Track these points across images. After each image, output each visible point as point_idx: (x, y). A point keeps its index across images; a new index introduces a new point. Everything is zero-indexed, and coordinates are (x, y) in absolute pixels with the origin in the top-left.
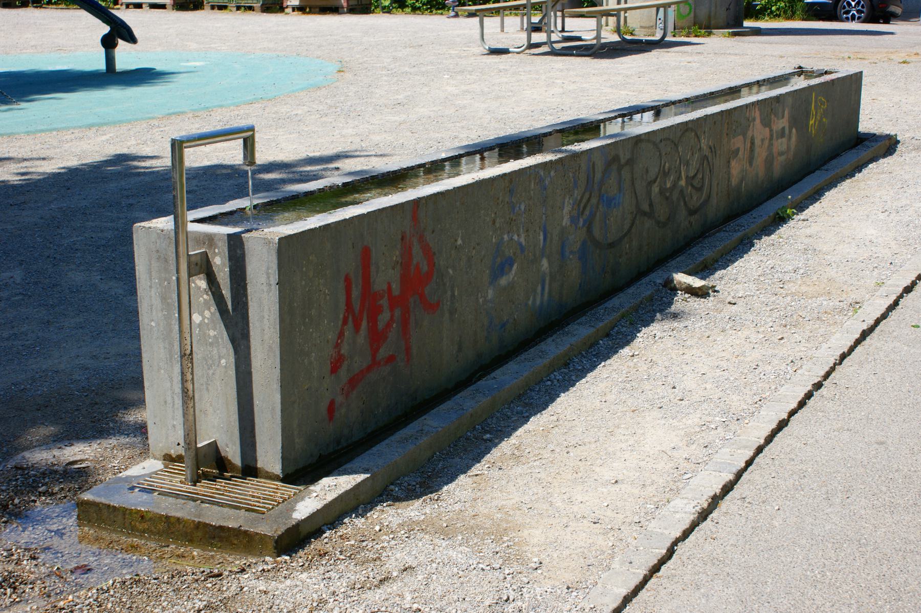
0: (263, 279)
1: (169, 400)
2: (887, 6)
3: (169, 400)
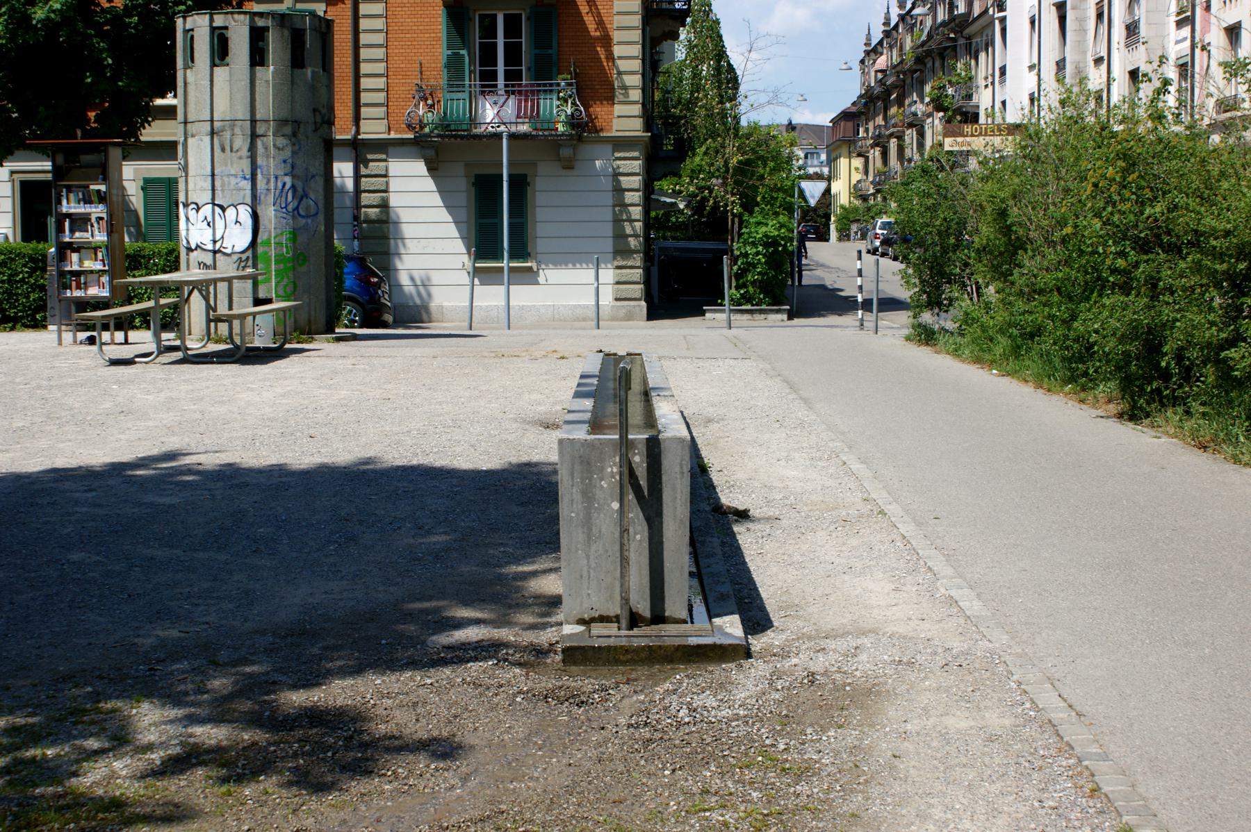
0: (677, 469)
1: (585, 574)
2: (381, 315)
3: (585, 574)
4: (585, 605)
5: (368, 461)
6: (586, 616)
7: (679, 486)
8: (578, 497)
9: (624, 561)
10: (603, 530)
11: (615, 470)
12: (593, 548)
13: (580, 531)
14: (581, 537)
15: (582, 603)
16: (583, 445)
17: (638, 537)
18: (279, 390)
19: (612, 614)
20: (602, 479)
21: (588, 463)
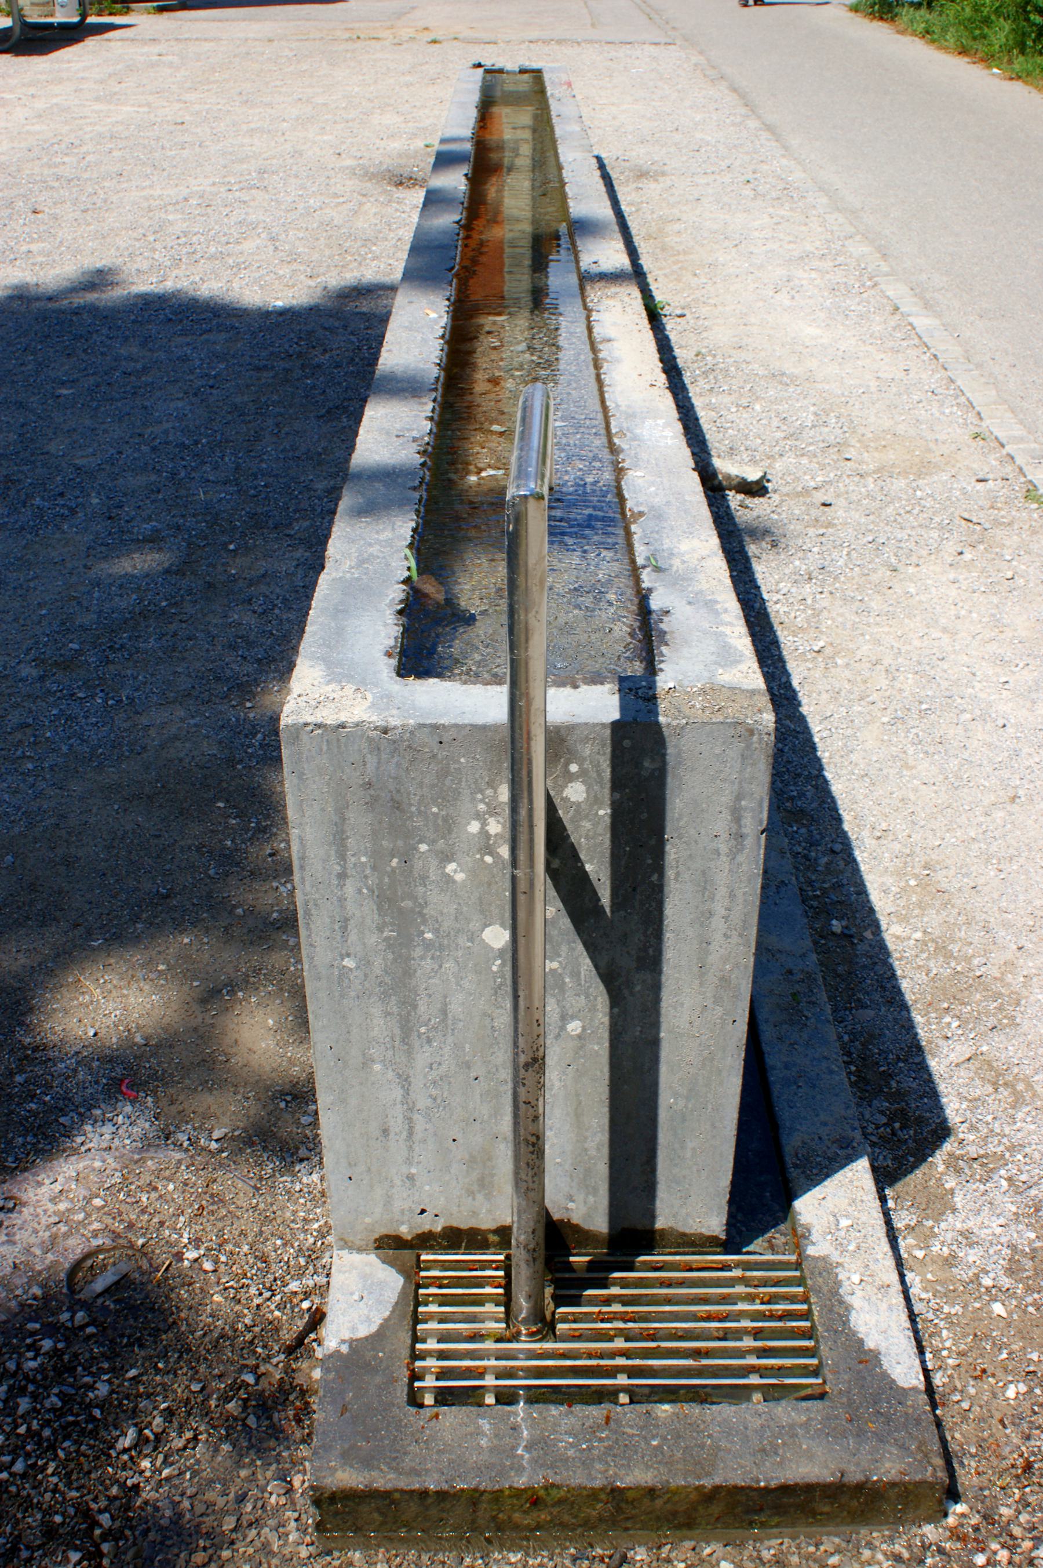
0: (721, 824)
1: (397, 1124)
4: (398, 1204)
5: (99, 279)
6: (405, 1231)
7: (722, 878)
8: (363, 910)
9: (530, 1065)
10: (455, 1008)
11: (495, 827)
12: (423, 1056)
13: (376, 1011)
14: (380, 1024)
15: (388, 1200)
16: (375, 747)
17: (574, 1027)
18: (40, 105)
19: (486, 1222)
20: (447, 857)
21: (397, 806)
